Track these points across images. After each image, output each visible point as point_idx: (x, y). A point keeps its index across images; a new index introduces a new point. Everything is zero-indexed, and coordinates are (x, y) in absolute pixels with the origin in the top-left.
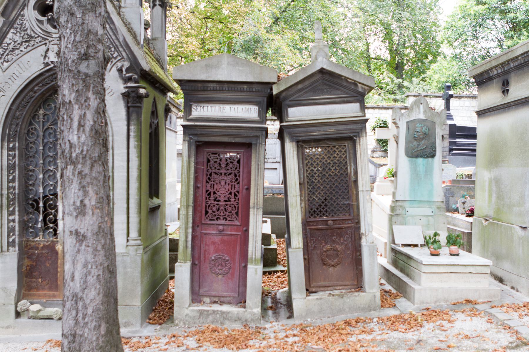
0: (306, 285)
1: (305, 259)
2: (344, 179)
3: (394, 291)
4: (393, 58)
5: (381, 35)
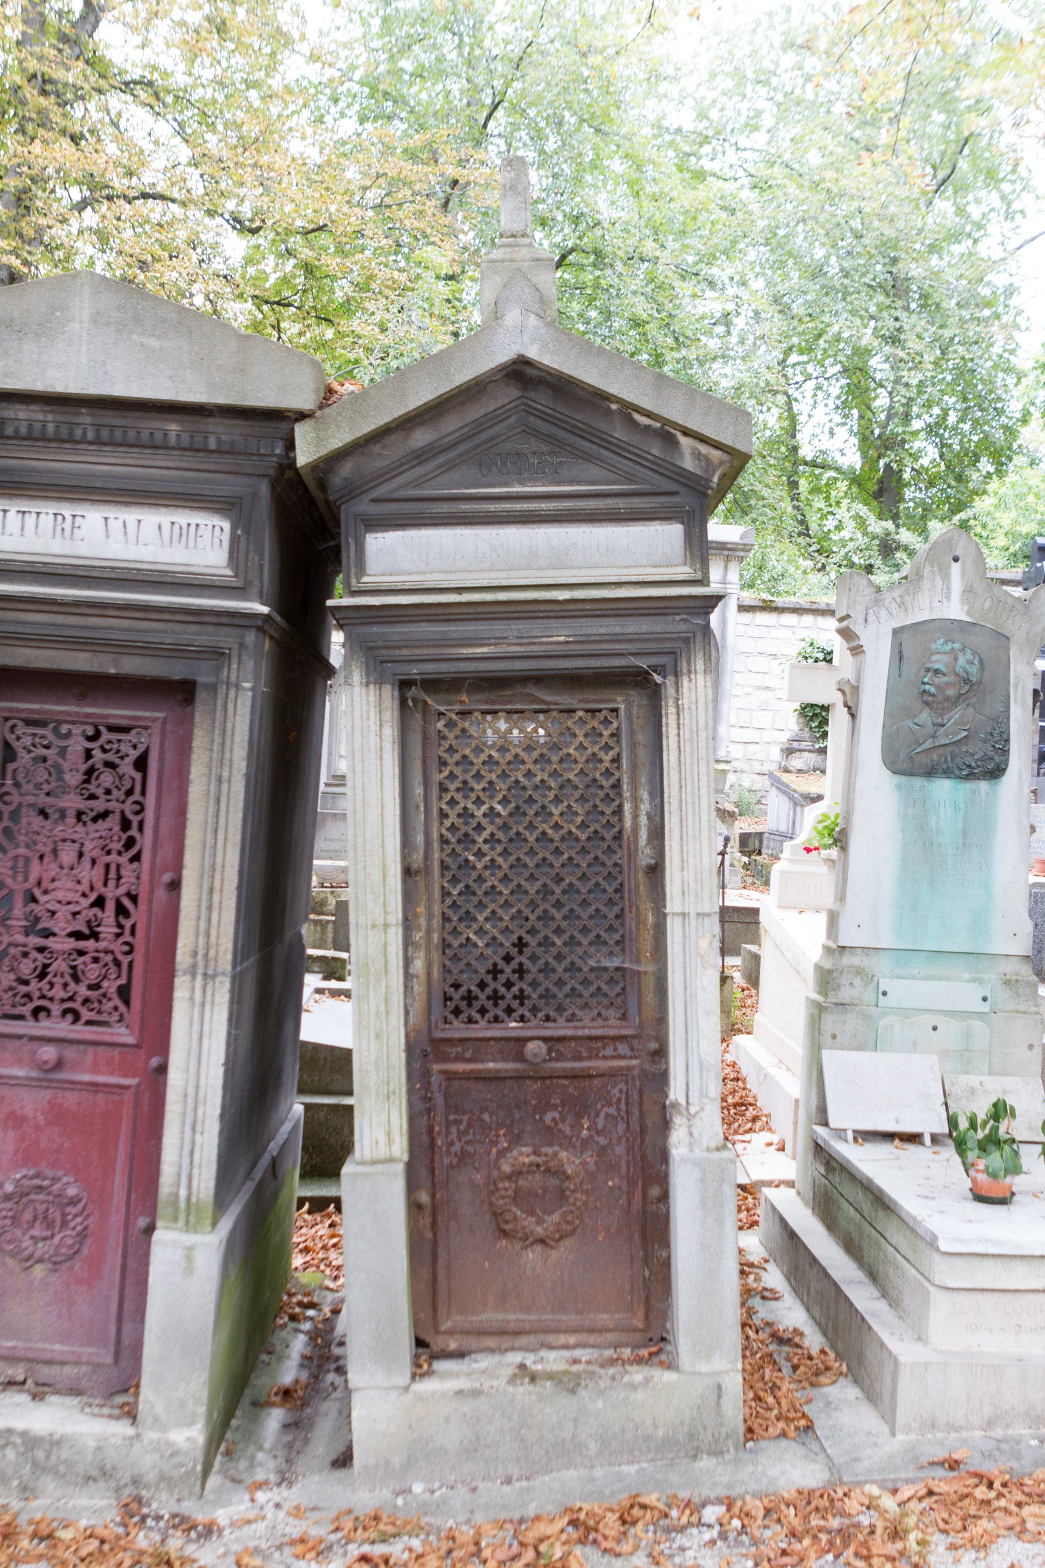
0: (416, 1323)
1: (414, 1207)
2: (603, 858)
3: (814, 1341)
4: (870, 463)
5: (835, 391)
